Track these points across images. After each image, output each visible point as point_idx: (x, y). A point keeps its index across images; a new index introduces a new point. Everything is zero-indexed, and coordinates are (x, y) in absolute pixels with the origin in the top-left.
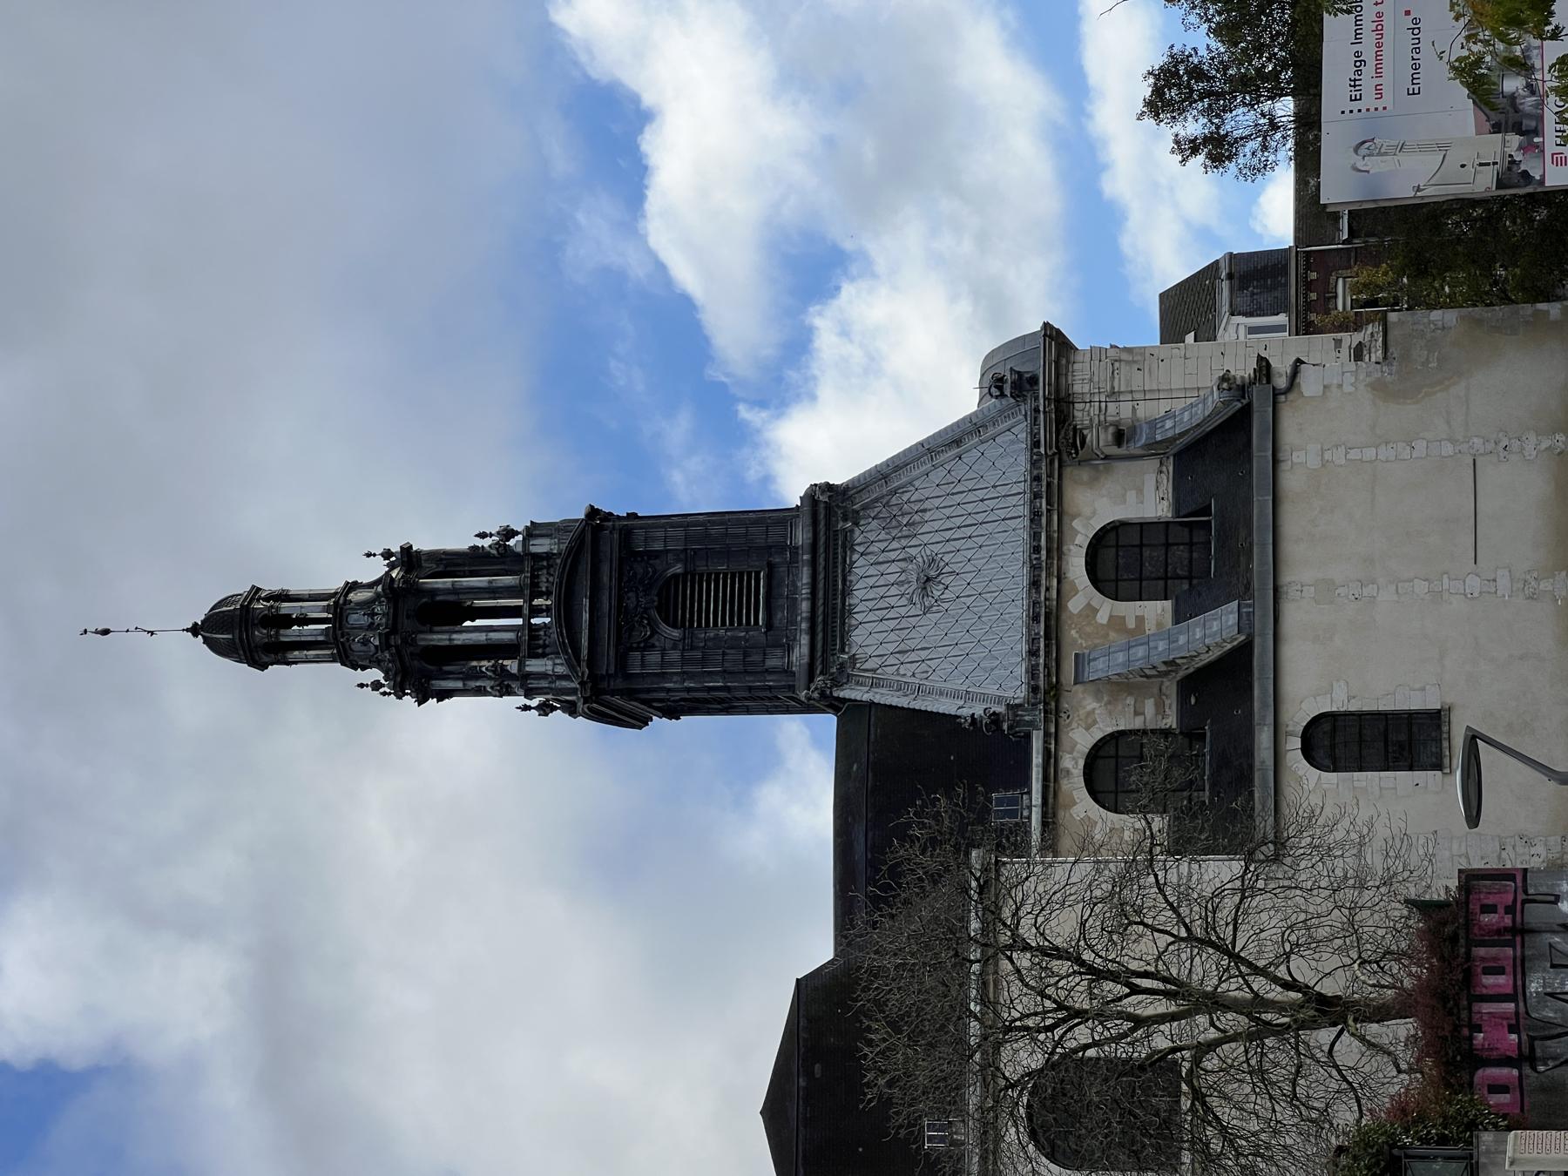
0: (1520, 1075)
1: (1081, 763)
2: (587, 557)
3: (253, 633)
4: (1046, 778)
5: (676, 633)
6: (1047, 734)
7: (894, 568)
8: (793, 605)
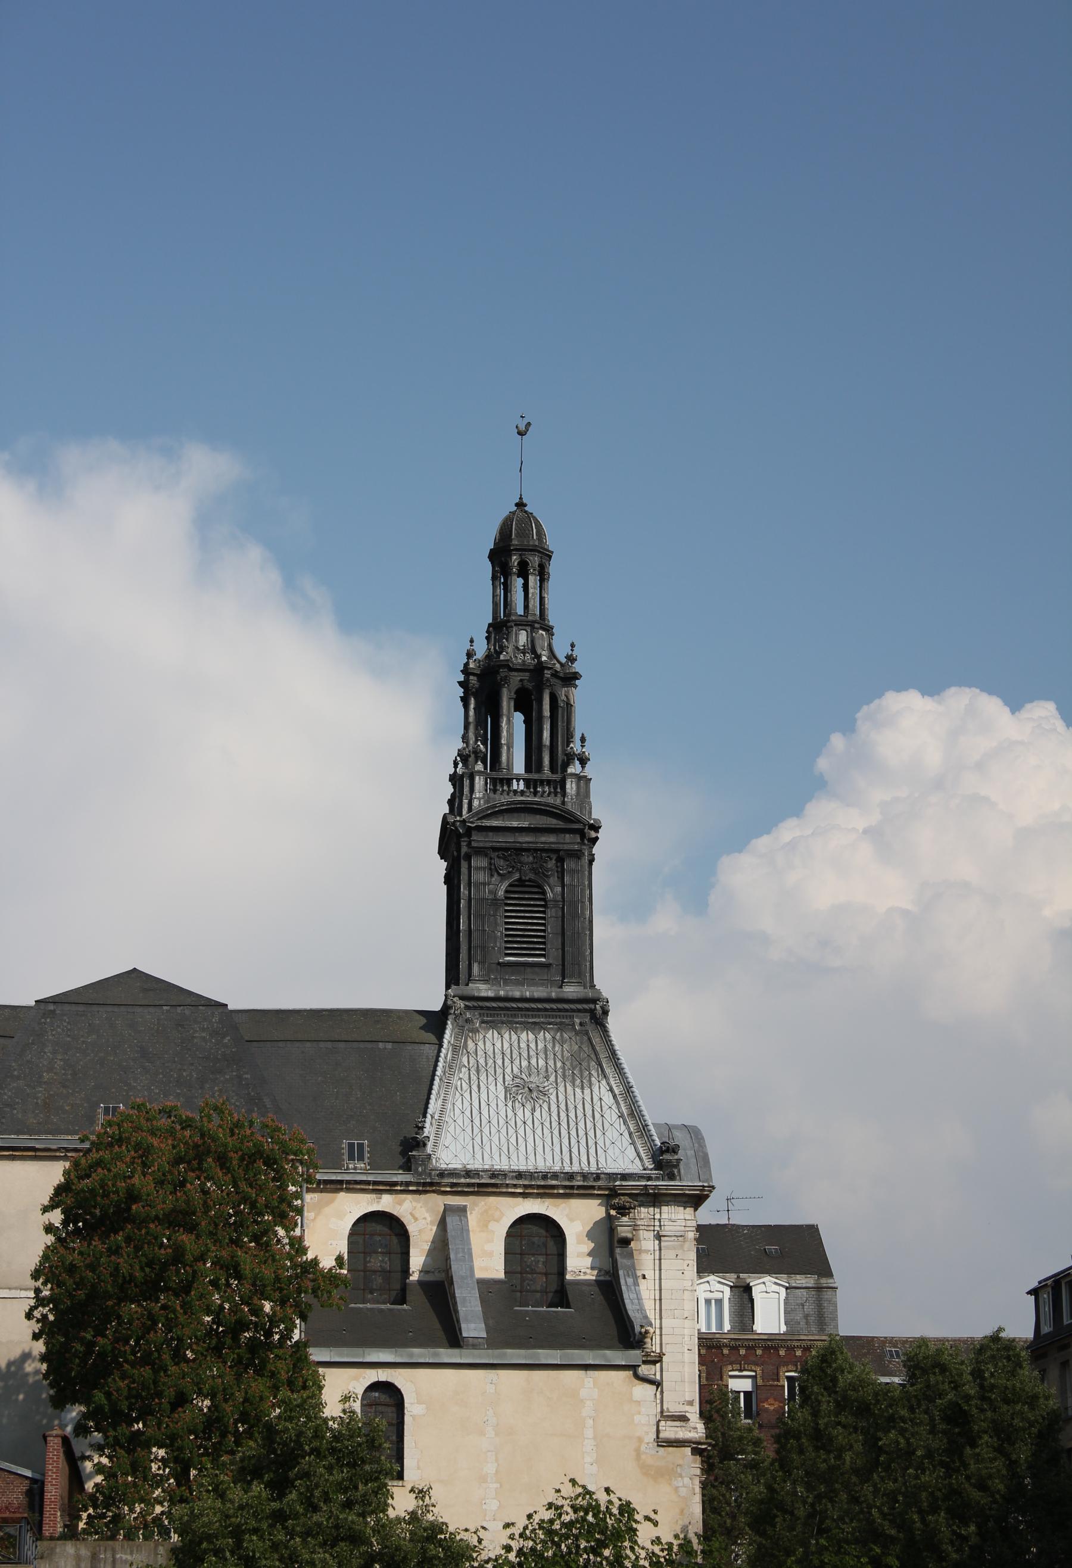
2: (560, 824)
3: (515, 554)
5: (501, 893)
6: (408, 1184)
7: (541, 1063)
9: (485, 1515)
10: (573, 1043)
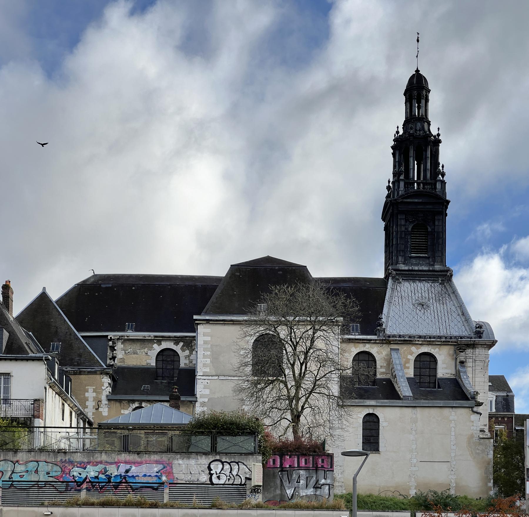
0: (277, 468)
1: (367, 350)
4: (363, 340)
5: (410, 229)
6: (376, 340)
7: (427, 295)
8: (417, 265)
9: (412, 465)
10: (439, 287)
